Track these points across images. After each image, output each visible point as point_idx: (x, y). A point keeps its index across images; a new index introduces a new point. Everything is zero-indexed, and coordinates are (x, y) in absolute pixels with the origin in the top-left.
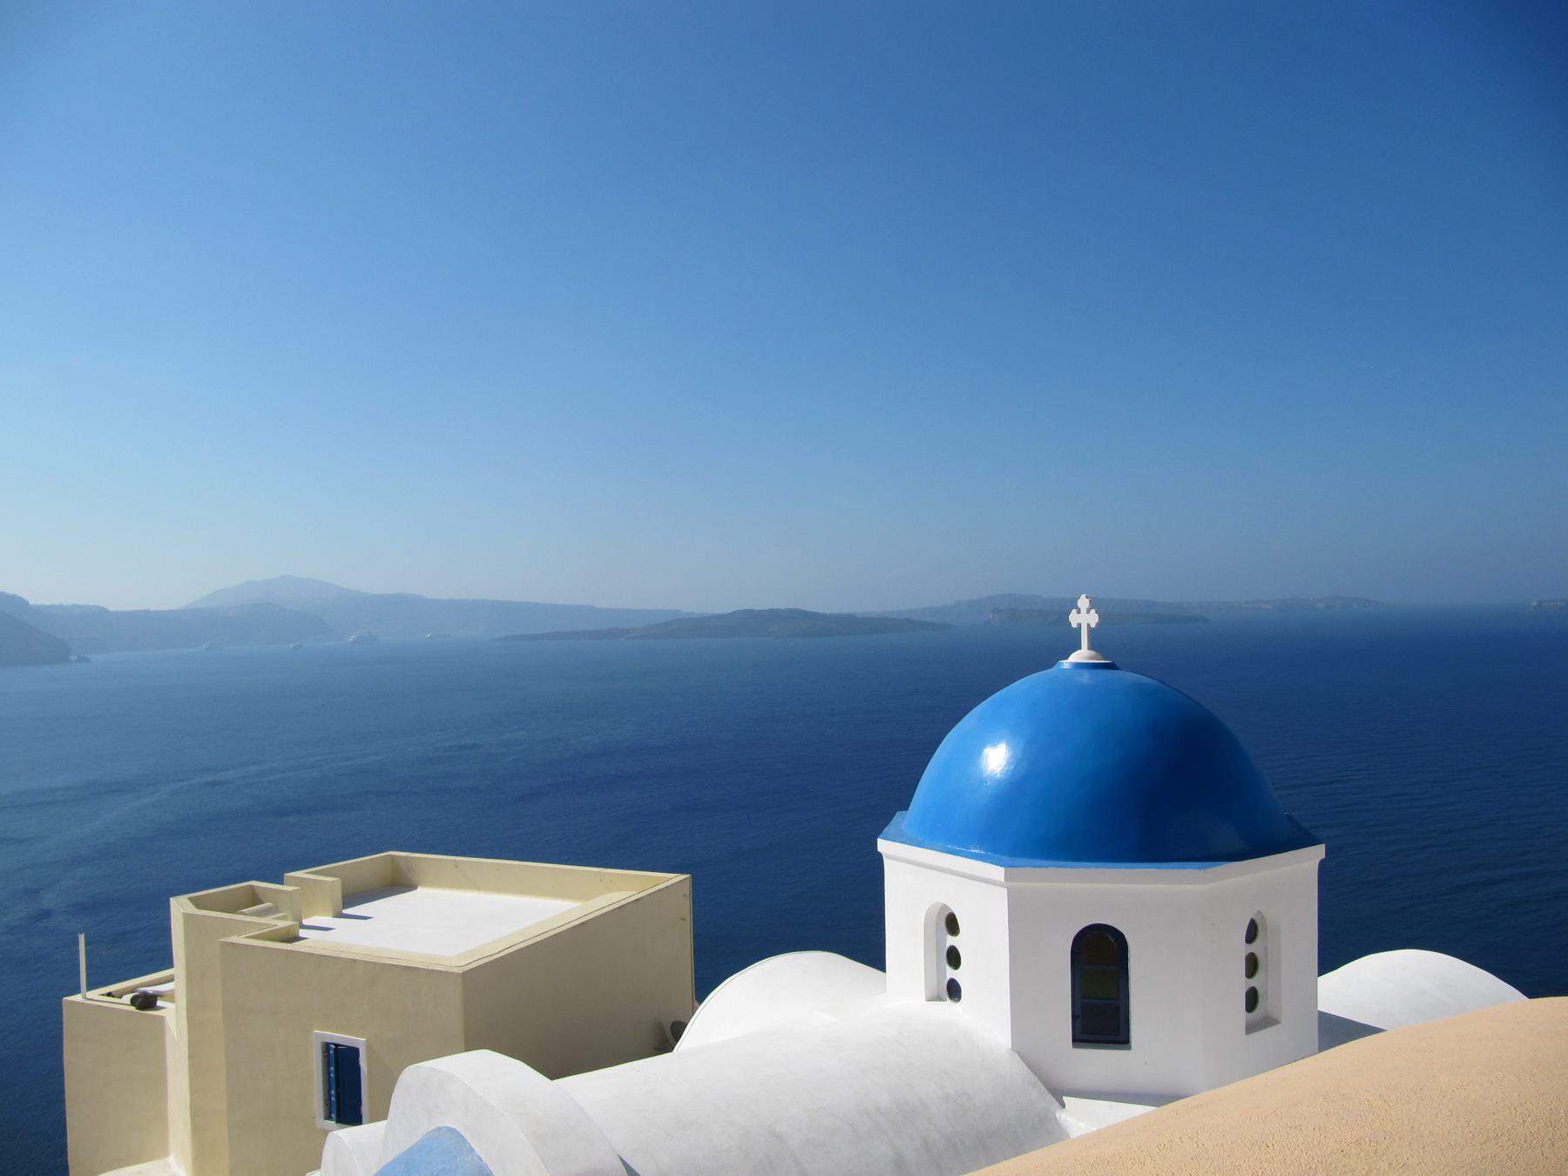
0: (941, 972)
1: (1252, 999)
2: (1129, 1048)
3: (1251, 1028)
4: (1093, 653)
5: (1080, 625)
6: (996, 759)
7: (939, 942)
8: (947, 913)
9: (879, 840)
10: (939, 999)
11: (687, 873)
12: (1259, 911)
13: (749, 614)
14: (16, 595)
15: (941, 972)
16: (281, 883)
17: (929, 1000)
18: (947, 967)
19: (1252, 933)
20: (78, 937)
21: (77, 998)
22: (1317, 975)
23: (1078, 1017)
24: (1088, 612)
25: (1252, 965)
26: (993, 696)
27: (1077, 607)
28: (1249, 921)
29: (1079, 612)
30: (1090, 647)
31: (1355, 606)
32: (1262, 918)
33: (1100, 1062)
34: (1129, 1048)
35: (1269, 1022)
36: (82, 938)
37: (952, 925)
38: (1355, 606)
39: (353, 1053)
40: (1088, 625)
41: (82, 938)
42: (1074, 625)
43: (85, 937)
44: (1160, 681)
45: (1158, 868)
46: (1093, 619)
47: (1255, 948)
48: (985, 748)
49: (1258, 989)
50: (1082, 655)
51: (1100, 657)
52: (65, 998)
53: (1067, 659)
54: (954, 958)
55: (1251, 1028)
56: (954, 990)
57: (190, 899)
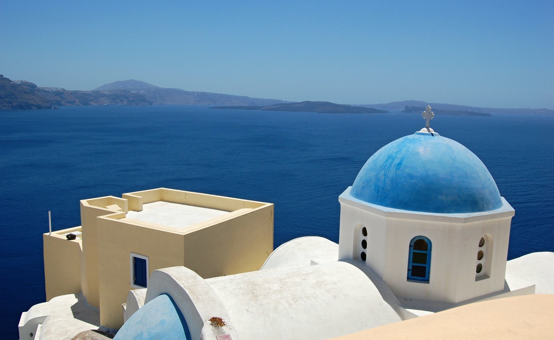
1: (479, 268)
2: (429, 283)
3: (478, 279)
8: (363, 227)
11: (273, 203)
12: (482, 238)
13: (308, 103)
16: (121, 197)
18: (512, 217)
19: (481, 244)
20: (48, 212)
21: (48, 234)
22: (505, 253)
23: (410, 270)
25: (480, 256)
32: (487, 237)
33: (417, 287)
34: (429, 283)
35: (486, 276)
36: (50, 212)
39: (144, 261)
41: (50, 212)
43: (51, 213)
47: (483, 249)
49: (482, 264)
52: (44, 234)
55: (478, 279)
57: (87, 201)
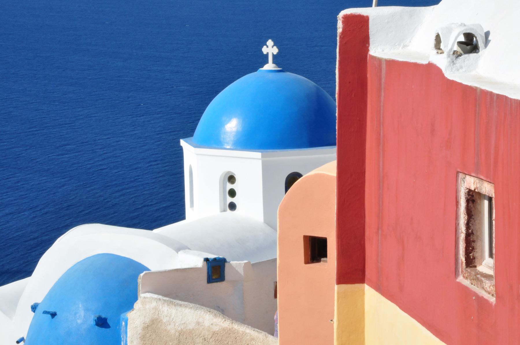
0: (225, 199)
2: (307, 262)
4: (274, 65)
5: (268, 53)
7: (224, 188)
10: (225, 211)
15: (225, 199)
17: (222, 212)
24: (273, 47)
27: (266, 45)
29: (267, 47)
30: (274, 62)
34: (307, 262)
37: (231, 179)
40: (273, 53)
42: (265, 53)
44: (96, 152)
45: (336, 231)
46: (275, 51)
50: (270, 66)
51: (277, 67)
53: (262, 67)
54: (232, 193)
56: (232, 206)
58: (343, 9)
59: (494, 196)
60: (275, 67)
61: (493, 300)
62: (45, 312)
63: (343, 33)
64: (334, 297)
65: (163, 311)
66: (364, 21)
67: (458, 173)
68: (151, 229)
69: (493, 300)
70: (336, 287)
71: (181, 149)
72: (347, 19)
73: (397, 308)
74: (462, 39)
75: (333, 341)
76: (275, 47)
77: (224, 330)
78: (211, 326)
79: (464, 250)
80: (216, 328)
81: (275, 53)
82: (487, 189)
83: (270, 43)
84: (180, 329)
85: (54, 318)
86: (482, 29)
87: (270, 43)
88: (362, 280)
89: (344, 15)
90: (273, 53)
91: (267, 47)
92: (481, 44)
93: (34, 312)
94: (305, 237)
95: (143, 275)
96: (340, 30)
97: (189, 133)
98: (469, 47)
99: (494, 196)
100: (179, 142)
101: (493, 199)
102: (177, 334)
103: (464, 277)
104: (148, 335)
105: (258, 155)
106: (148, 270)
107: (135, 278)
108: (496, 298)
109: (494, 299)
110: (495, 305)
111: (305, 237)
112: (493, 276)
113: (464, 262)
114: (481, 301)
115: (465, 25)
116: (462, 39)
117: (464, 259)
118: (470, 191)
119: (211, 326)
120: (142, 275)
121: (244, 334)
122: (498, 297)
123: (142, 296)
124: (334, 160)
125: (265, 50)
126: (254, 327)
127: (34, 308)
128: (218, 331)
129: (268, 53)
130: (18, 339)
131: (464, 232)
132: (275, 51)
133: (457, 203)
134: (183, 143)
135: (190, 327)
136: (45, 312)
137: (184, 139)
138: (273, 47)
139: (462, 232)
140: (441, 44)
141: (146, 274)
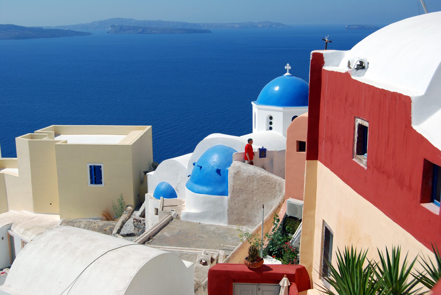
4: (289, 74)
5: (287, 69)
6: (277, 88)
9: (415, 127)
10: (268, 130)
14: (416, 130)
24: (289, 66)
26: (276, 78)
27: (286, 65)
28: (17, 157)
29: (287, 66)
31: (274, 26)
34: (297, 151)
37: (271, 118)
38: (274, 26)
40: (289, 69)
42: (286, 69)
46: (290, 68)
48: (279, 89)
50: (287, 74)
54: (271, 123)
56: (271, 128)
58: (313, 50)
59: (368, 127)
60: (290, 74)
61: (366, 168)
62: (198, 166)
63: (312, 60)
64: (305, 165)
65: (242, 168)
66: (320, 56)
67: (355, 117)
68: (239, 136)
69: (366, 168)
70: (306, 161)
71: (252, 105)
72: (314, 54)
73: (329, 170)
74: (359, 63)
75: (304, 182)
76: (290, 66)
77: (265, 176)
78: (260, 174)
79: (356, 148)
80: (262, 175)
81: (290, 69)
82: (366, 124)
83: (288, 65)
84: (248, 175)
85: (156, 188)
86: (367, 61)
87: (288, 65)
88: (317, 159)
89: (313, 53)
90: (289, 69)
91: (287, 66)
92: (366, 67)
93: (194, 166)
94: (297, 141)
95: (235, 154)
96: (311, 59)
97: (255, 99)
98: (361, 67)
99: (368, 127)
100: (251, 103)
101: (368, 128)
102: (247, 177)
103: (355, 158)
104: (236, 177)
105: (281, 108)
106: (236, 151)
107: (232, 154)
108: (367, 167)
109: (366, 167)
110: (366, 170)
111: (297, 141)
112: (367, 127)
113: (356, 153)
114: (362, 168)
115: (360, 58)
116: (359, 63)
117: (356, 152)
118: (359, 124)
119: (260, 174)
120: (234, 153)
121: (273, 178)
122: (368, 167)
123: (234, 162)
124: (307, 112)
125: (286, 67)
126: (277, 176)
127: (194, 164)
128: (263, 176)
129: (287, 69)
130: (188, 175)
131: (357, 141)
132: (290, 68)
133: (354, 129)
134: (252, 103)
135: (253, 174)
136: (198, 166)
137: (254, 102)
138: (289, 66)
139: (356, 141)
140: (350, 65)
141: (235, 153)
